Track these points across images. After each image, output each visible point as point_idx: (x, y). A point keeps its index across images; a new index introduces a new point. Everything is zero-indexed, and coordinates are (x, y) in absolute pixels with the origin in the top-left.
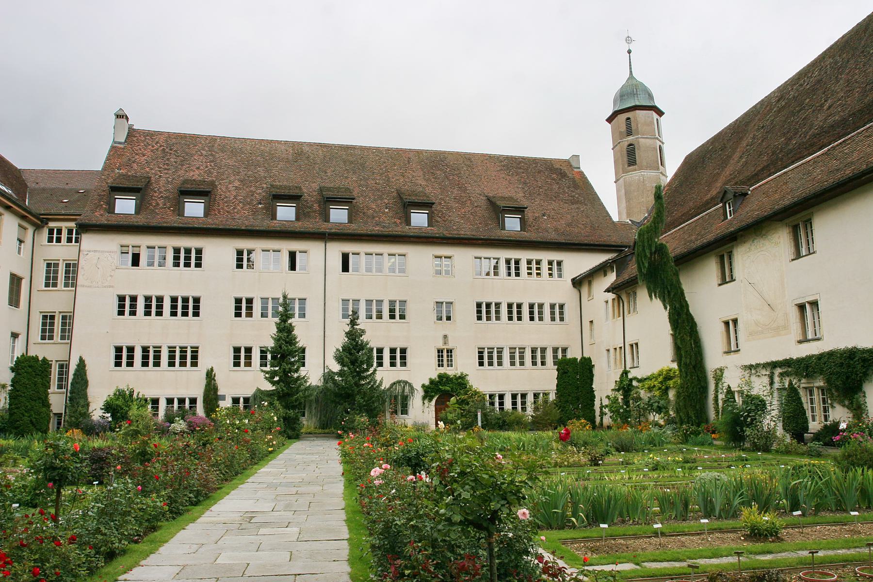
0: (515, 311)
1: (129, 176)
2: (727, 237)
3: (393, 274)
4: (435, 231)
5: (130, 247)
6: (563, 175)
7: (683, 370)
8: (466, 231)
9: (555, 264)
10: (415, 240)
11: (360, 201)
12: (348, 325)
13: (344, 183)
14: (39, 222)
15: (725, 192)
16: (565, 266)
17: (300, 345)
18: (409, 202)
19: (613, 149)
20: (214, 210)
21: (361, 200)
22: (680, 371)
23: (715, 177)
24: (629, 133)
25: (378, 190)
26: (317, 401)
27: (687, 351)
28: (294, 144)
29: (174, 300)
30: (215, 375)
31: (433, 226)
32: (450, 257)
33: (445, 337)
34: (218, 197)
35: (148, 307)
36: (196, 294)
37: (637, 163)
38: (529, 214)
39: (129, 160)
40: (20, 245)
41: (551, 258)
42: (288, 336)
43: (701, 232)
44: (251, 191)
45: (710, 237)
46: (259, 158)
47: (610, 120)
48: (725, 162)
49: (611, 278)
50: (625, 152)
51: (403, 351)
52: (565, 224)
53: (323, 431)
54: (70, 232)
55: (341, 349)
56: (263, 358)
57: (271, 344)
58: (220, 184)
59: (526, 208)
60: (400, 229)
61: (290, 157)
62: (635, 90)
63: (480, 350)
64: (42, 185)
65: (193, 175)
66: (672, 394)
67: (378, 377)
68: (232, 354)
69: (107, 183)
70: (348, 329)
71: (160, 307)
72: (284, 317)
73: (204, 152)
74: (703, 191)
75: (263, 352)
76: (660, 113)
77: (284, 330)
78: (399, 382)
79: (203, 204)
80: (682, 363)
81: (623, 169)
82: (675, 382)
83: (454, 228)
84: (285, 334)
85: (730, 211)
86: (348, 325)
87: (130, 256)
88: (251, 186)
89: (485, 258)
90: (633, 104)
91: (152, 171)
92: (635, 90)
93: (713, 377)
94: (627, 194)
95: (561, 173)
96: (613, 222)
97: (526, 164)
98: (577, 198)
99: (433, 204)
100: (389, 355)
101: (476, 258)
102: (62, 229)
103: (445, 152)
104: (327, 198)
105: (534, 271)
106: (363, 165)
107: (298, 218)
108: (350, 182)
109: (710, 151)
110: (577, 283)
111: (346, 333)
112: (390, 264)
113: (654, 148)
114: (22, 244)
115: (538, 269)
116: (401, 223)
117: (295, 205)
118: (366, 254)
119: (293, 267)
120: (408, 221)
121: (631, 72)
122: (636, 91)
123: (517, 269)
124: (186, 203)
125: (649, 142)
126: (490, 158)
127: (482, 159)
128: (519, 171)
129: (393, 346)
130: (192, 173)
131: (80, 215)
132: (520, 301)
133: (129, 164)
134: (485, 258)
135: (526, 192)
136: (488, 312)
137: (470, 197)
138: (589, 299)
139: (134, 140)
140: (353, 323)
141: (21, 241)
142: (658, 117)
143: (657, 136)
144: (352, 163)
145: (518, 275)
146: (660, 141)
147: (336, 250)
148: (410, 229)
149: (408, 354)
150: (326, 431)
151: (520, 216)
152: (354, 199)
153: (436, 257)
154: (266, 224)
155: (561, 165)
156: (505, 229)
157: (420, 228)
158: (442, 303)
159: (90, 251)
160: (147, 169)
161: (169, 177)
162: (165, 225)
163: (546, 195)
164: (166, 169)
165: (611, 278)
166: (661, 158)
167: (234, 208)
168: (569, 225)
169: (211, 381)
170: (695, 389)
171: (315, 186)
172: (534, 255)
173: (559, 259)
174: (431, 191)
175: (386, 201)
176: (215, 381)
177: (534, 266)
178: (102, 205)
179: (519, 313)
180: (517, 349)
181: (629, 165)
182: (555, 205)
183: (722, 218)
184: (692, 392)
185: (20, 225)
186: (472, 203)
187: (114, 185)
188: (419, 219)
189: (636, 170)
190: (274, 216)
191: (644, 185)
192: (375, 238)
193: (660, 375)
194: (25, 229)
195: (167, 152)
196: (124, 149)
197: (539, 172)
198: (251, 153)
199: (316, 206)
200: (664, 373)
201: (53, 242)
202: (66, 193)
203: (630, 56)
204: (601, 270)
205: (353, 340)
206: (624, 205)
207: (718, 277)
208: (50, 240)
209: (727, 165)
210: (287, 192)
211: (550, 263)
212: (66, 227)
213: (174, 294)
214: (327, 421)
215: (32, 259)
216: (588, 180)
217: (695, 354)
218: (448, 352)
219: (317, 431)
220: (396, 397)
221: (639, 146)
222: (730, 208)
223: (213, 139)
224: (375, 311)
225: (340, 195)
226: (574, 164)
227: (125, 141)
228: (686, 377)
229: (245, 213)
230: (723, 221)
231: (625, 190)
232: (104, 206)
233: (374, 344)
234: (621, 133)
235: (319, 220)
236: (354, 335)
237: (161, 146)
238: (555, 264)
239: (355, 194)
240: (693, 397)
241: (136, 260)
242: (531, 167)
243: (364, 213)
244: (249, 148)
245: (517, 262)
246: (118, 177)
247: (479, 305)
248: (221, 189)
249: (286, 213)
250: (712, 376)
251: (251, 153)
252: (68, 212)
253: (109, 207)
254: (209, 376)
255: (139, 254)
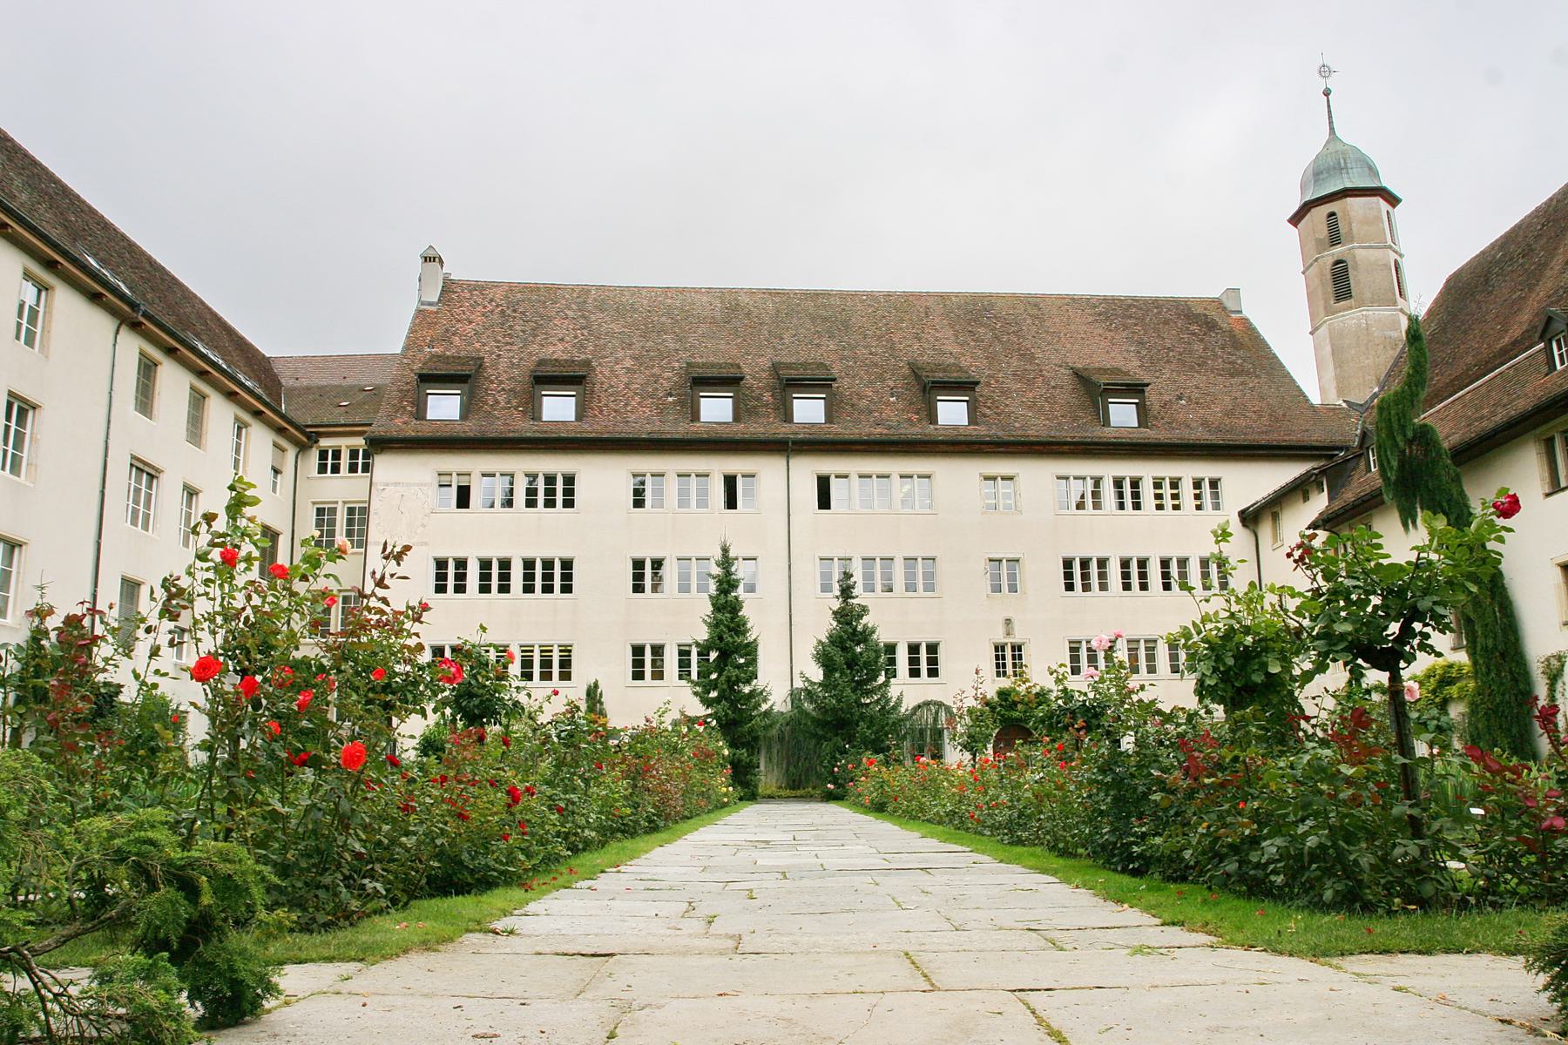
0: (1134, 573)
1: (448, 357)
2: (1561, 400)
3: (910, 511)
4: (981, 431)
5: (454, 475)
6: (1211, 326)
7: (1481, 661)
8: (1038, 428)
9: (1206, 485)
10: (945, 448)
11: (843, 385)
12: (837, 597)
13: (814, 355)
14: (305, 439)
15: (1549, 320)
16: (1224, 487)
17: (751, 637)
18: (933, 382)
19: (1303, 273)
20: (592, 409)
21: (846, 382)
22: (1475, 663)
23: (1515, 306)
24: (1335, 239)
25: (876, 365)
26: (781, 739)
27: (1487, 625)
28: (722, 293)
29: (529, 565)
30: (601, 694)
31: (977, 424)
32: (1011, 478)
33: (1008, 622)
34: (597, 386)
35: (485, 577)
36: (566, 555)
37: (1353, 294)
38: (1151, 396)
39: (447, 331)
40: (275, 477)
41: (1199, 475)
42: (732, 619)
43: (1501, 400)
44: (654, 375)
45: (1523, 404)
46: (664, 319)
47: (1295, 220)
48: (1532, 278)
49: (1319, 503)
50: (1329, 276)
51: (933, 648)
52: (1221, 412)
53: (794, 793)
54: (354, 454)
55: (825, 640)
56: (684, 664)
57: (703, 634)
58: (600, 364)
59: (1147, 385)
60: (917, 430)
61: (718, 315)
62: (1342, 161)
63: (1073, 645)
64: (305, 382)
65: (554, 352)
66: (1456, 711)
67: (893, 692)
68: (630, 658)
69: (412, 370)
70: (836, 605)
71: (505, 577)
72: (726, 586)
73: (570, 313)
74: (1491, 332)
75: (684, 654)
76: (1393, 200)
77: (724, 608)
78: (927, 704)
79: (574, 398)
80: (1479, 648)
81: (1326, 308)
82: (1461, 689)
83: (1017, 425)
84: (728, 615)
85: (1561, 356)
86: (837, 597)
87: (454, 491)
88: (654, 366)
89: (1075, 478)
90: (1339, 187)
91: (484, 348)
92: (1342, 161)
93: (1543, 673)
94: (1338, 354)
95: (1207, 323)
96: (1312, 406)
97: (1141, 309)
98: (1241, 365)
99: (977, 383)
100: (907, 656)
101: (1058, 478)
102: (340, 451)
103: (990, 295)
104: (788, 380)
105: (1168, 502)
106: (846, 325)
107: (737, 417)
108: (826, 353)
109: (1500, 261)
110: (1250, 518)
111: (834, 613)
112: (902, 495)
113: (1385, 265)
114: (279, 476)
115: (1175, 497)
116: (919, 420)
117: (731, 394)
118: (860, 477)
119: (731, 503)
120: (932, 417)
121: (1332, 129)
122: (1345, 163)
123: (1136, 495)
124: (545, 398)
125: (1374, 255)
126: (1074, 300)
127: (1059, 303)
128: (1129, 321)
129: (915, 640)
130: (551, 349)
131: (370, 425)
132: (1143, 555)
133: (446, 338)
134: (1075, 478)
135: (1143, 358)
136: (1085, 576)
137: (1041, 371)
138: (1275, 546)
139: (453, 299)
140: (846, 592)
141: (276, 471)
142: (1390, 208)
143: (1389, 242)
144: (825, 319)
145: (1137, 506)
146: (1396, 252)
147: (806, 470)
148: (936, 429)
149: (942, 655)
150: (799, 793)
151: (1137, 401)
152: (834, 380)
153: (987, 478)
154: (681, 429)
155: (1205, 309)
156: (1109, 425)
157: (956, 428)
158: (1000, 561)
159: (388, 485)
160: (477, 345)
161: (513, 357)
162: (511, 435)
163: (1182, 362)
164: (507, 344)
165: (1319, 503)
166: (1399, 283)
167: (626, 405)
168: (1229, 413)
169: (595, 705)
170: (1507, 696)
171: (765, 362)
172: (1167, 469)
173: (1215, 475)
174: (972, 363)
175: (891, 383)
176: (602, 704)
177: (1167, 491)
178: (404, 407)
179: (1143, 575)
180: (1142, 642)
181: (1338, 300)
182: (1199, 379)
183: (1545, 369)
184: (1502, 702)
185: (275, 445)
186: (1046, 382)
187: (424, 372)
188: (952, 413)
189: (1351, 308)
190: (695, 416)
191: (1368, 335)
192: (877, 448)
193: (1429, 677)
194: (283, 450)
195: (509, 316)
196: (437, 313)
197: (1166, 323)
198: (649, 311)
199: (767, 396)
200: (1438, 672)
201: (326, 472)
202: (345, 392)
203: (1328, 101)
204: (1298, 490)
205: (848, 624)
206: (1330, 372)
207: (1542, 480)
208: (322, 469)
209: (1538, 281)
210: (713, 373)
211: (1197, 484)
212: (347, 447)
213: (529, 554)
214: (800, 775)
215: (294, 501)
216: (1258, 333)
217: (1504, 631)
218: (1013, 649)
219: (783, 793)
220: (922, 732)
221: (1356, 263)
222: (1560, 348)
223: (585, 291)
224: (879, 578)
225: (809, 373)
226: (1230, 305)
227: (439, 300)
228: (1488, 674)
229: (644, 412)
230: (1547, 375)
231: (1332, 345)
232: (409, 408)
233: (883, 637)
234: (1319, 241)
235: (775, 418)
236: (847, 616)
237: (497, 306)
238: (1206, 485)
239: (835, 372)
240: (1503, 712)
241: (463, 498)
242: (1150, 314)
243: (853, 405)
244: (645, 302)
245: (1135, 484)
246: (430, 359)
247: (1068, 564)
248: (601, 374)
249: (716, 409)
250: (1541, 670)
251: (649, 311)
252: (350, 421)
253: (417, 410)
254: (592, 695)
255: (469, 487)
